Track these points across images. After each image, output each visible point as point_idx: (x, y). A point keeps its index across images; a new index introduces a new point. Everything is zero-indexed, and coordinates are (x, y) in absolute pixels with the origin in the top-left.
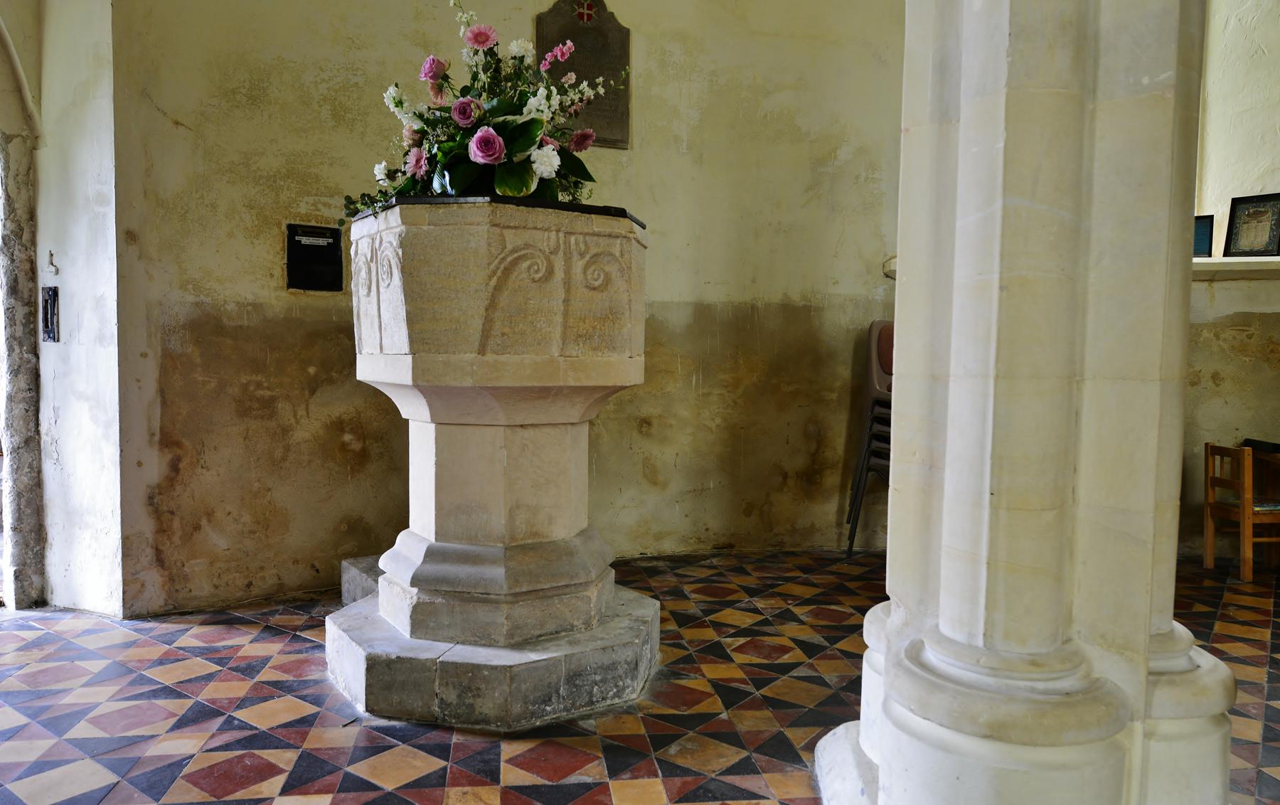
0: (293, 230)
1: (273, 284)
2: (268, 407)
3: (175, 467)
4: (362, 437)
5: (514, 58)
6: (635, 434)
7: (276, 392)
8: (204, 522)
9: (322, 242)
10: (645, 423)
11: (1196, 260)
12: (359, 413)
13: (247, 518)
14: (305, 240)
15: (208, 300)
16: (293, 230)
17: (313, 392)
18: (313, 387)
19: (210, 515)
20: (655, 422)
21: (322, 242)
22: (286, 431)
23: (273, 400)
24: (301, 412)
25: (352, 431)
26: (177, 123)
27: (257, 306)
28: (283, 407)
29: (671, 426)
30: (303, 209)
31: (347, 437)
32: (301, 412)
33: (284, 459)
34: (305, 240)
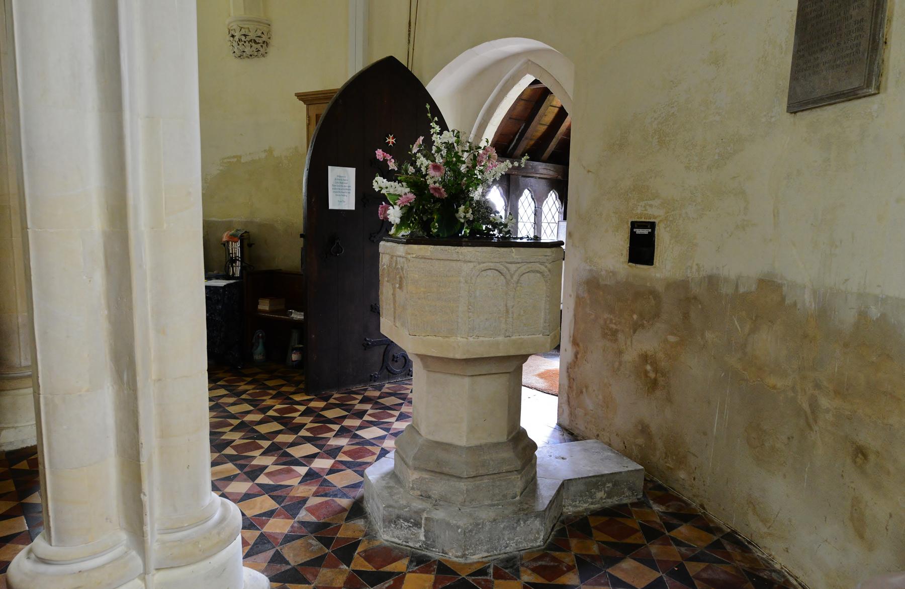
0: (634, 225)
1: (622, 260)
2: (615, 333)
3: (576, 355)
4: (656, 370)
5: (265, 151)
6: (849, 461)
7: (619, 327)
8: (584, 390)
9: (646, 231)
10: (860, 453)
11: (529, 79)
12: (655, 353)
13: (600, 397)
14: (639, 231)
15: (594, 268)
16: (634, 225)
17: (634, 332)
18: (636, 327)
19: (587, 387)
20: (872, 457)
21: (646, 231)
22: (621, 353)
23: (617, 331)
24: (629, 343)
25: (651, 365)
26: (589, 171)
27: (614, 273)
28: (620, 336)
29: (889, 473)
30: (639, 210)
31: (648, 367)
32: (629, 343)
33: (619, 369)
34: (639, 231)
